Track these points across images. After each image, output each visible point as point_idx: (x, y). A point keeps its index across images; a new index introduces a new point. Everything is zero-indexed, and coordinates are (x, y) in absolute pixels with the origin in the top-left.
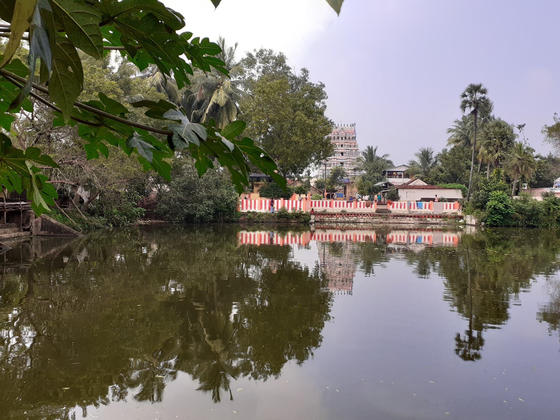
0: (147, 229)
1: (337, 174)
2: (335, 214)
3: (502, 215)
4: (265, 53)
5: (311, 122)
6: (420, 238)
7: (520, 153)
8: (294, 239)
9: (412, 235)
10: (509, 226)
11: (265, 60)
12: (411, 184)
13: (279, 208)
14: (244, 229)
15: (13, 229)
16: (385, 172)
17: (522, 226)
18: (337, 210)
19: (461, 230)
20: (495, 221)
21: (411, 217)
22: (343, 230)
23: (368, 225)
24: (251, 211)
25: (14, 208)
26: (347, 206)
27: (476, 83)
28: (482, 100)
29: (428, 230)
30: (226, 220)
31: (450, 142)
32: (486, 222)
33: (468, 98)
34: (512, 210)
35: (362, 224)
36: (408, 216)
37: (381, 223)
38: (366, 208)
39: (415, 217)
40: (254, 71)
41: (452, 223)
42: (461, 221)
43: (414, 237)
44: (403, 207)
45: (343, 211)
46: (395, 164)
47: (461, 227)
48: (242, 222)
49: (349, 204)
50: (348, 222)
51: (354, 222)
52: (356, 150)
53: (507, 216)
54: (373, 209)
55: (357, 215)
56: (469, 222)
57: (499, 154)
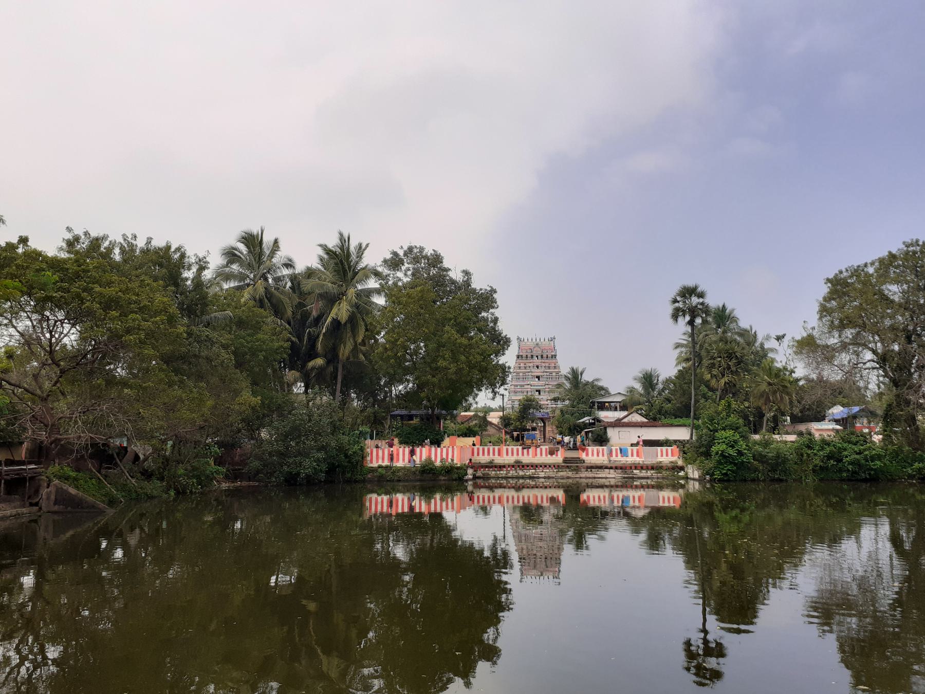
0: (233, 493)
1: (528, 407)
2: (504, 467)
3: (735, 464)
4: (415, 251)
5: (464, 341)
6: (628, 498)
7: (770, 376)
8: (444, 504)
9: (615, 494)
10: (745, 481)
11: (416, 260)
12: (626, 420)
13: (424, 458)
14: (372, 492)
15: (13, 505)
16: (593, 403)
17: (764, 481)
18: (509, 459)
19: (683, 486)
20: (726, 474)
21: (611, 468)
22: (518, 488)
23: (551, 480)
24: (384, 464)
25: (18, 474)
26: (523, 454)
27: (690, 284)
28: (699, 307)
29: (636, 487)
30: (345, 478)
31: (680, 361)
32: (712, 475)
33: (680, 305)
34: (748, 457)
35: (543, 480)
36: (606, 468)
37: (568, 478)
38: (549, 456)
39: (616, 468)
40: (400, 274)
41: (669, 477)
42: (682, 474)
43: (618, 497)
44: (601, 454)
45: (517, 462)
46: (613, 391)
47: (682, 482)
48: (370, 481)
49: (525, 451)
50: (523, 478)
51: (531, 478)
52: (557, 373)
53: (741, 466)
54: (558, 458)
55: (535, 466)
56: (690, 475)
57: (726, 379)
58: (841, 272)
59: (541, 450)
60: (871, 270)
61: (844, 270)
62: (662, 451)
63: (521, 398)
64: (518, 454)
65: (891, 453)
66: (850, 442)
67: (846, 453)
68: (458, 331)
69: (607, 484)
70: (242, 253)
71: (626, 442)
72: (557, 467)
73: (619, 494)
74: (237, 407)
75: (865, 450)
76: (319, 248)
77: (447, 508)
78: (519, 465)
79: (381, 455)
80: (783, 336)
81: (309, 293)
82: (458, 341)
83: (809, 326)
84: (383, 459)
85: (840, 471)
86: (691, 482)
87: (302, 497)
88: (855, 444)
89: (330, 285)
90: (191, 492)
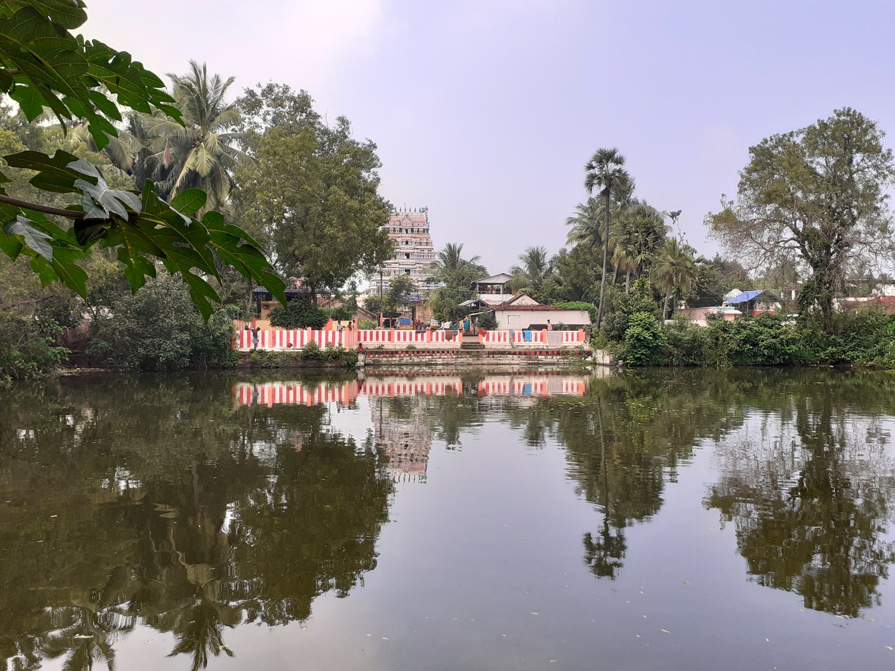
1: (401, 287)
2: (397, 352)
3: (649, 348)
4: (276, 90)
5: (355, 204)
10: (658, 365)
11: (278, 102)
12: (514, 303)
13: (306, 342)
14: (244, 380)
16: (474, 285)
17: (678, 366)
18: (399, 344)
19: (589, 373)
20: (639, 358)
21: (515, 354)
22: (411, 377)
23: (450, 367)
26: (416, 339)
27: (608, 148)
29: (541, 374)
30: (212, 365)
33: (596, 171)
35: (440, 367)
36: (510, 353)
37: (469, 364)
38: (446, 341)
39: (520, 353)
40: (257, 119)
41: (576, 362)
42: (589, 359)
44: (502, 339)
45: (410, 347)
46: (491, 272)
47: (589, 368)
48: (242, 368)
49: (419, 335)
50: (418, 364)
51: (427, 364)
52: (430, 250)
53: (655, 350)
54: (456, 343)
55: (431, 352)
56: (600, 360)
58: (766, 141)
59: (437, 334)
60: (798, 140)
61: (769, 139)
62: (567, 335)
64: (411, 339)
65: (806, 337)
66: (765, 326)
67: (762, 337)
69: (510, 371)
75: (780, 334)
81: (154, 137)
85: (755, 355)
86: (601, 368)
88: (770, 328)
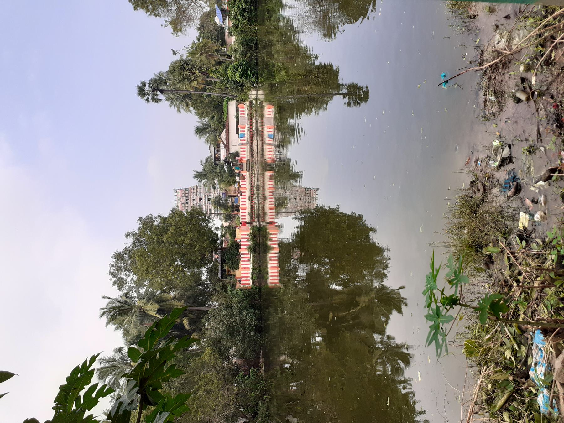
1: (218, 203)
2: (252, 206)
3: (247, 69)
6: (269, 135)
8: (274, 239)
11: (119, 269)
14: (266, 282)
17: (257, 53)
19: (261, 103)
20: (253, 75)
21: (252, 143)
22: (265, 198)
23: (259, 178)
24: (251, 276)
27: (136, 90)
30: (259, 298)
32: (254, 83)
33: (150, 97)
34: (244, 61)
36: (252, 146)
37: (258, 168)
39: (252, 140)
40: (129, 279)
41: (256, 109)
42: (254, 102)
44: (244, 150)
45: (249, 198)
47: (259, 102)
48: (260, 284)
49: (243, 194)
50: (258, 194)
51: (258, 190)
52: (197, 188)
53: (248, 65)
54: (247, 174)
56: (254, 96)
57: (197, 72)
63: (213, 208)
66: (234, 4)
68: (166, 233)
69: (261, 145)
70: (111, 379)
71: (237, 142)
72: (251, 175)
73: (266, 139)
74: (212, 361)
76: (109, 326)
77: (276, 237)
78: (251, 198)
79: (245, 273)
80: (173, 51)
82: (173, 231)
83: (165, 24)
84: (247, 277)
85: (251, 10)
87: (269, 322)
89: (134, 317)
90: (265, 386)
